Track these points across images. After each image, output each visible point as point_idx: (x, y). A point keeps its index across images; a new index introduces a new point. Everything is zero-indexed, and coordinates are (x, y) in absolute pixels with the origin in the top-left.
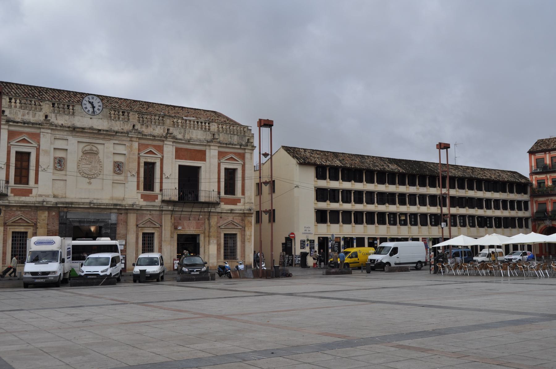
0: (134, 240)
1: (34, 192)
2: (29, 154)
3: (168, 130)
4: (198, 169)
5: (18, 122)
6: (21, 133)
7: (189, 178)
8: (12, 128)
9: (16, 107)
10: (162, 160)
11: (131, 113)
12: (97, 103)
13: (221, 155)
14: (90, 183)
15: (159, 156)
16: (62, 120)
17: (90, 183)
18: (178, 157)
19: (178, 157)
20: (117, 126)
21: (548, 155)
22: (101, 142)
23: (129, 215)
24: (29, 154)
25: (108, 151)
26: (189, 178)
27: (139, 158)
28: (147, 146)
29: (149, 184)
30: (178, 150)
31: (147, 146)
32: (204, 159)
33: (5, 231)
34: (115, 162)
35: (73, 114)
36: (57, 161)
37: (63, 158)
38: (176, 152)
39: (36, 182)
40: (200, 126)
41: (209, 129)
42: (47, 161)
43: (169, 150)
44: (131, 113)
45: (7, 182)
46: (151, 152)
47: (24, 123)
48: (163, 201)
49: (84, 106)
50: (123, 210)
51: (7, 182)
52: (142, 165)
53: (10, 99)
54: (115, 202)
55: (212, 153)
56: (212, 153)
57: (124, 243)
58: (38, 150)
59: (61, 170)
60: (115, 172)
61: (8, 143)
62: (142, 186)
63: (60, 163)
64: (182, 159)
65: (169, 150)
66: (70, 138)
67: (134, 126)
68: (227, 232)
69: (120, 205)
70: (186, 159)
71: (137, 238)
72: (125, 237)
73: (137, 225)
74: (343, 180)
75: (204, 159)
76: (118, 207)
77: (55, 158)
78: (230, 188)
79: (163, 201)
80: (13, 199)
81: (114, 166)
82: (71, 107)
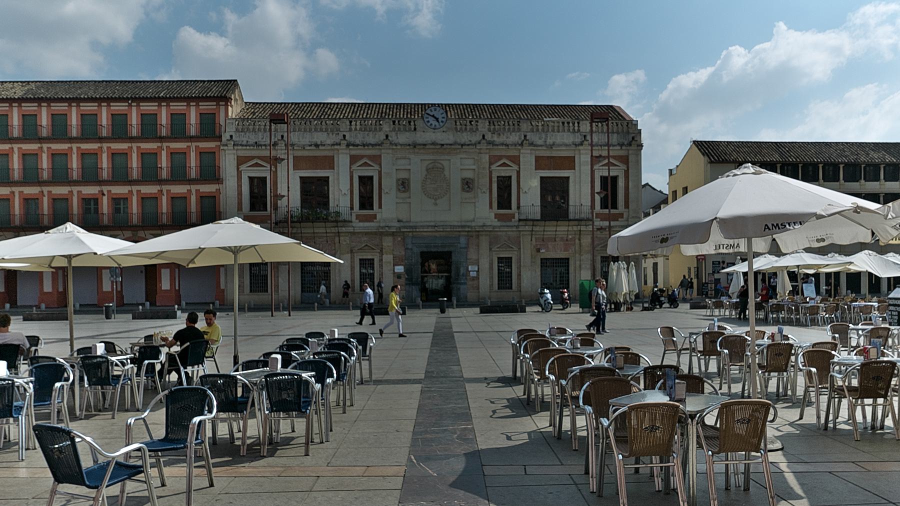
0: (487, 266)
1: (378, 217)
2: (371, 178)
3: (525, 136)
4: (326, 180)
5: (357, 145)
6: (362, 157)
7: (555, 193)
8: (353, 152)
9: (356, 129)
10: (518, 173)
11: (480, 121)
12: (439, 113)
13: (354, 159)
14: (436, 204)
15: (515, 167)
16: (404, 138)
17: (436, 204)
18: (538, 167)
19: (538, 167)
20: (465, 138)
21: (104, 110)
22: (447, 157)
23: (481, 238)
24: (371, 178)
25: (458, 166)
26: (555, 193)
27: (491, 172)
28: (500, 158)
29: (504, 201)
30: (538, 159)
31: (500, 158)
32: (332, 167)
33: (352, 258)
34: (463, 179)
35: (415, 129)
36: (400, 182)
37: (473, 180)
38: (536, 161)
39: (380, 207)
40: (566, 128)
41: (579, 130)
42: (389, 184)
43: (528, 159)
44: (480, 121)
45: (352, 208)
46: (504, 165)
47: (364, 145)
48: (520, 220)
49: (426, 120)
50: (474, 233)
51: (352, 208)
52: (495, 179)
53: (351, 122)
54: (463, 224)
55: (343, 160)
56: (343, 160)
57: (476, 269)
58: (380, 173)
59: (404, 192)
60: (463, 189)
61: (238, 169)
62: (495, 205)
63: (404, 185)
64: (544, 169)
65: (528, 159)
66: (412, 156)
67: (484, 136)
68: (365, 257)
69: (469, 227)
70: (549, 169)
71: (491, 264)
72: (477, 263)
73: (490, 249)
74: (886, 180)
75: (332, 167)
76: (467, 229)
77: (398, 180)
78: (366, 202)
79: (520, 220)
80: (359, 226)
81: (463, 183)
82: (412, 123)
